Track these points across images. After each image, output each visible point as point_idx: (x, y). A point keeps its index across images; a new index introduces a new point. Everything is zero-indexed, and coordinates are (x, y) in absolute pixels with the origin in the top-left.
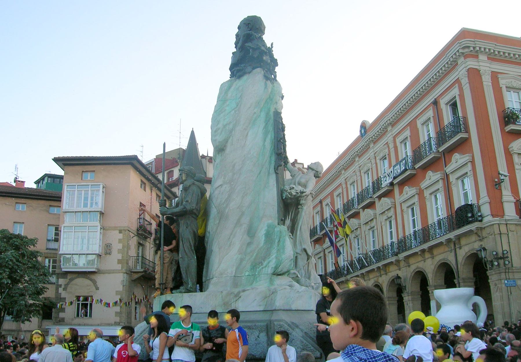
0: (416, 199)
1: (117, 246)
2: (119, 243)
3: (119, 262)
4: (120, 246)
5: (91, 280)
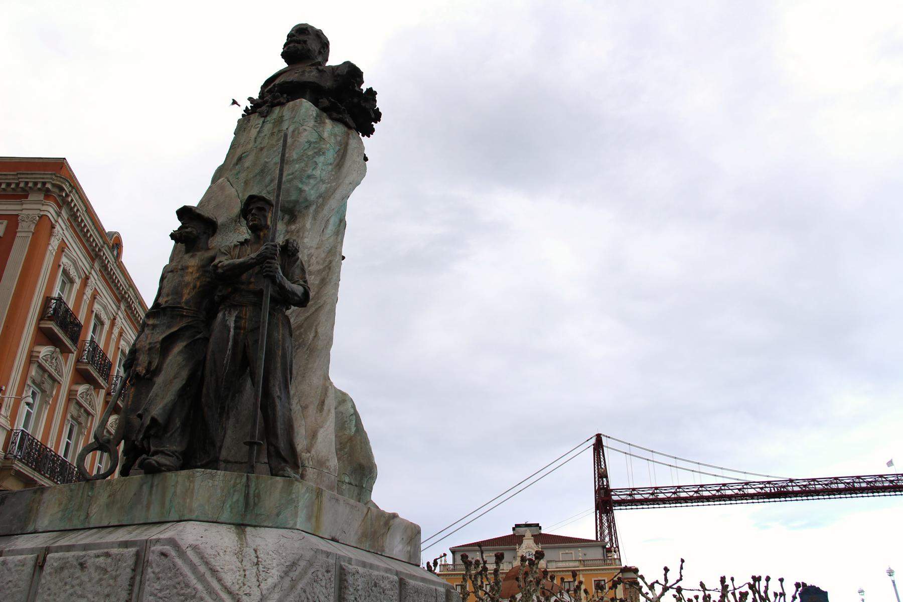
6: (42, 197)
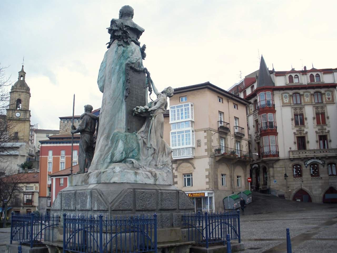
1: (204, 141)
2: (205, 138)
3: (206, 150)
4: (206, 141)
5: (191, 163)
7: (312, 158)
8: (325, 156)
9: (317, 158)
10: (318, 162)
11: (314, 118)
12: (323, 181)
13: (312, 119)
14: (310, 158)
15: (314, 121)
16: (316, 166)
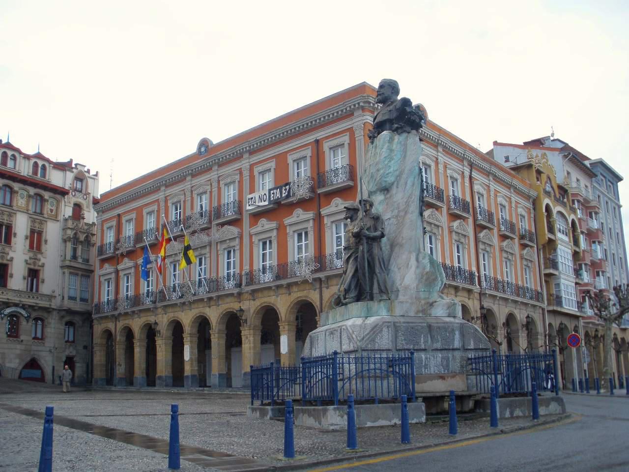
0: (113, 276)
6: (360, 112)
7: (16, 305)
8: (35, 305)
9: (24, 307)
10: (20, 313)
11: (26, 238)
12: (23, 347)
13: (24, 237)
14: (12, 304)
15: (25, 241)
16: (15, 319)
